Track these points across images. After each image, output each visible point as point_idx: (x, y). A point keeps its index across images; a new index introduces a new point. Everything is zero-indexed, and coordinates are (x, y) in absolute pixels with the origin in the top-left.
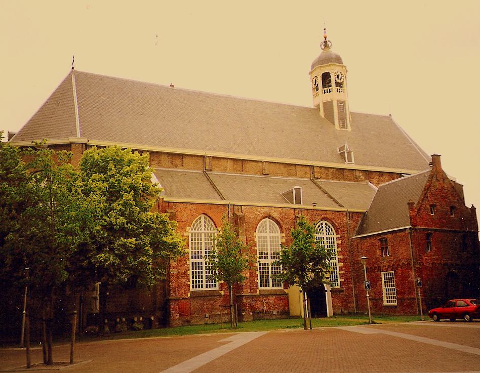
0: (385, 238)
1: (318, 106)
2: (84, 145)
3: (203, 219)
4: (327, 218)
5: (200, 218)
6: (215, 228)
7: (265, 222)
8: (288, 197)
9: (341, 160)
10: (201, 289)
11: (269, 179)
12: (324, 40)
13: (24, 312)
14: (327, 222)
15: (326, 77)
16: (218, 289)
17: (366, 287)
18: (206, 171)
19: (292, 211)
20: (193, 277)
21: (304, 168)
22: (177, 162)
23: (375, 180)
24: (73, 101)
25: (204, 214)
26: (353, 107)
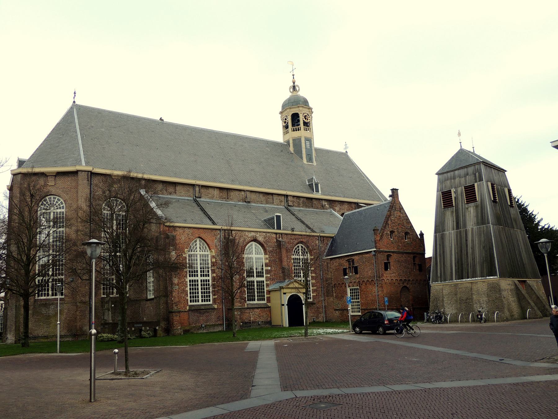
0: (352, 259)
1: (288, 142)
2: (89, 173)
3: (198, 242)
4: (302, 242)
5: (196, 241)
6: (208, 250)
7: (252, 245)
8: (269, 223)
9: (310, 191)
10: (197, 303)
11: (251, 206)
12: (292, 84)
13: (59, 322)
14: (304, 246)
15: (295, 117)
16: (212, 303)
17: (348, 302)
18: (196, 198)
19: (274, 236)
20: (190, 293)
21: (280, 197)
22: (171, 189)
23: (337, 208)
24: (76, 132)
25: (199, 237)
26: (318, 143)
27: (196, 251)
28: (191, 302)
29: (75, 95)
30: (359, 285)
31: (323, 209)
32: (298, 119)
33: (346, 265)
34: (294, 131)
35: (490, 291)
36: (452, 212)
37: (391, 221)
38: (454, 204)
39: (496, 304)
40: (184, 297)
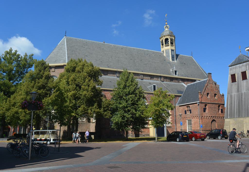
29: (66, 33)
31: (179, 83)
34: (166, 46)
37: (208, 88)
38: (237, 81)
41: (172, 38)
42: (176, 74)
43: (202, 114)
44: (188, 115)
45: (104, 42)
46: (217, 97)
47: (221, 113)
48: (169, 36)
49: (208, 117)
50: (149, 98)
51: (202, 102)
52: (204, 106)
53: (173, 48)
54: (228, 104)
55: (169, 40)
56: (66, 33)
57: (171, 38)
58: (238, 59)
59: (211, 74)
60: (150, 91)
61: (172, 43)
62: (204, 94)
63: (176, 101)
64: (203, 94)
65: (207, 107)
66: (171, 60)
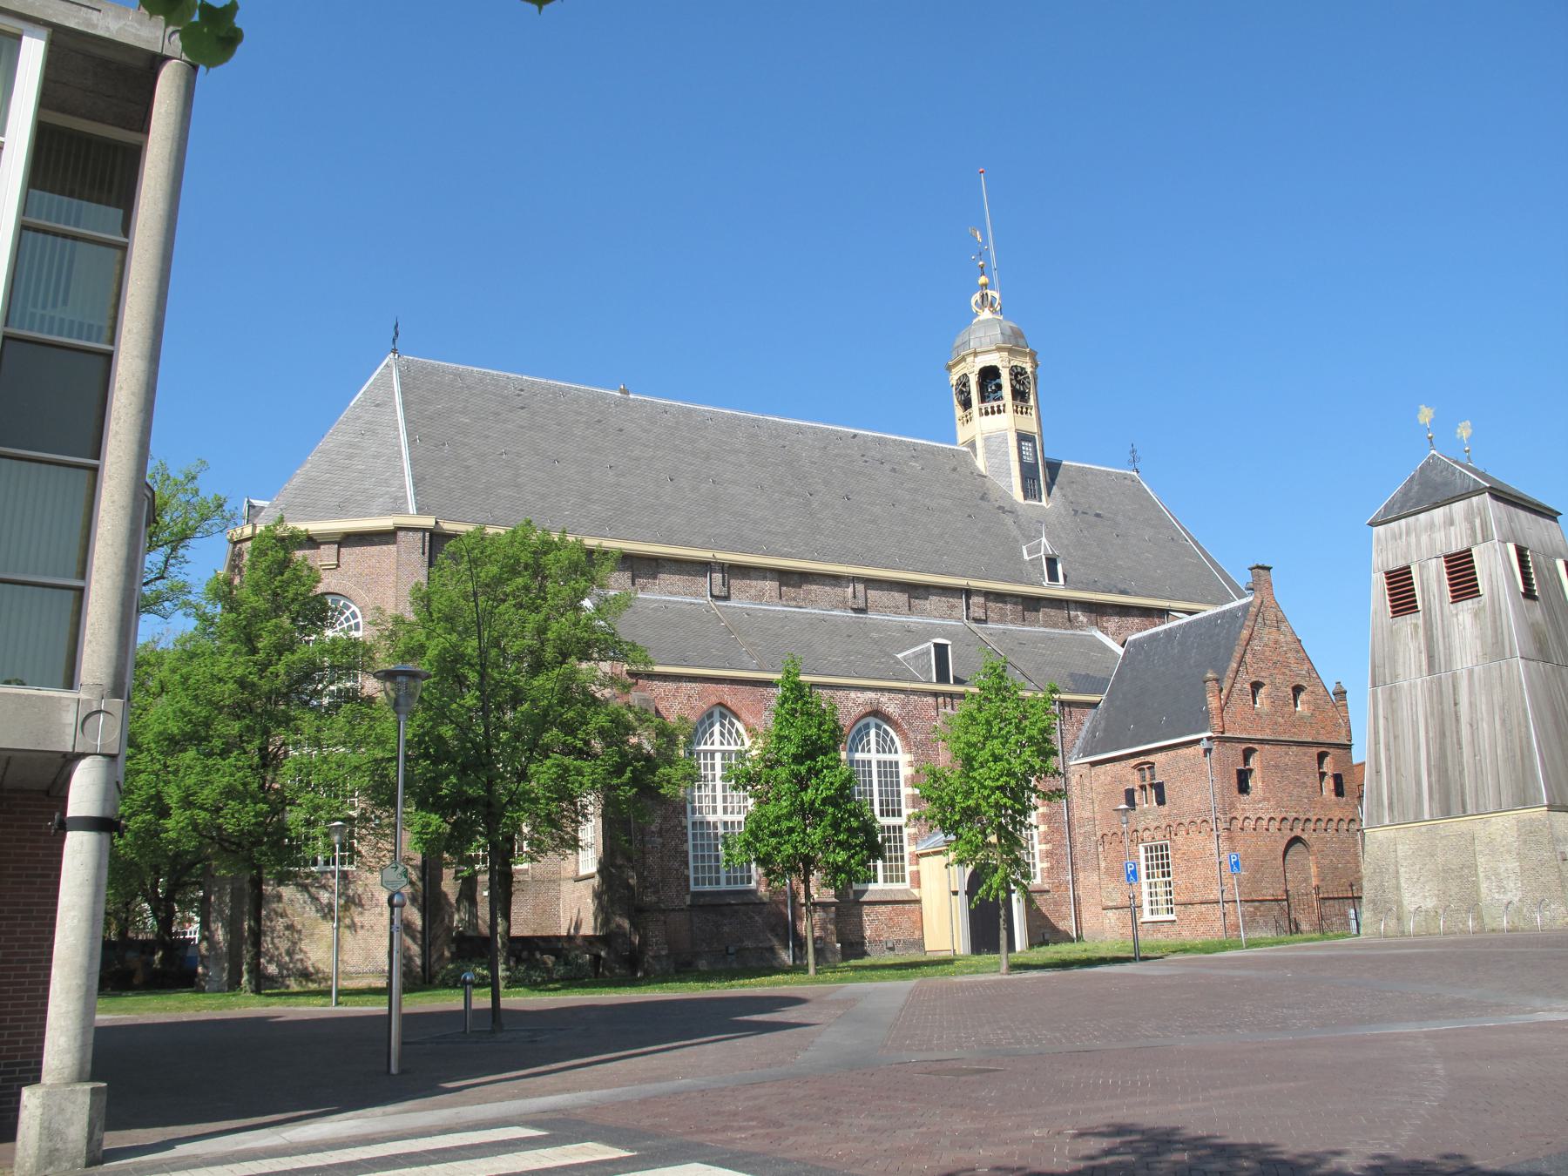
2: (427, 534)
10: (714, 888)
20: (695, 857)
24: (397, 429)
27: (712, 744)
28: (697, 883)
29: (397, 334)
30: (1168, 836)
32: (997, 381)
33: (1134, 780)
34: (987, 413)
35: (1525, 842)
36: (1416, 626)
38: (1419, 604)
39: (1542, 879)
40: (677, 870)
41: (1017, 362)
42: (1053, 576)
43: (1232, 806)
44: (1144, 813)
45: (625, 392)
46: (1308, 702)
47: (1333, 796)
48: (1005, 354)
49: (1264, 823)
50: (917, 723)
51: (1226, 735)
52: (1241, 758)
53: (1030, 424)
54: (1377, 743)
55: (1005, 379)
56: (397, 334)
57: (1014, 363)
58: (1420, 484)
59: (1269, 569)
60: (916, 680)
61: (1019, 395)
62: (1238, 686)
63: (1069, 737)
64: (1232, 686)
65: (1254, 763)
66: (1018, 494)
